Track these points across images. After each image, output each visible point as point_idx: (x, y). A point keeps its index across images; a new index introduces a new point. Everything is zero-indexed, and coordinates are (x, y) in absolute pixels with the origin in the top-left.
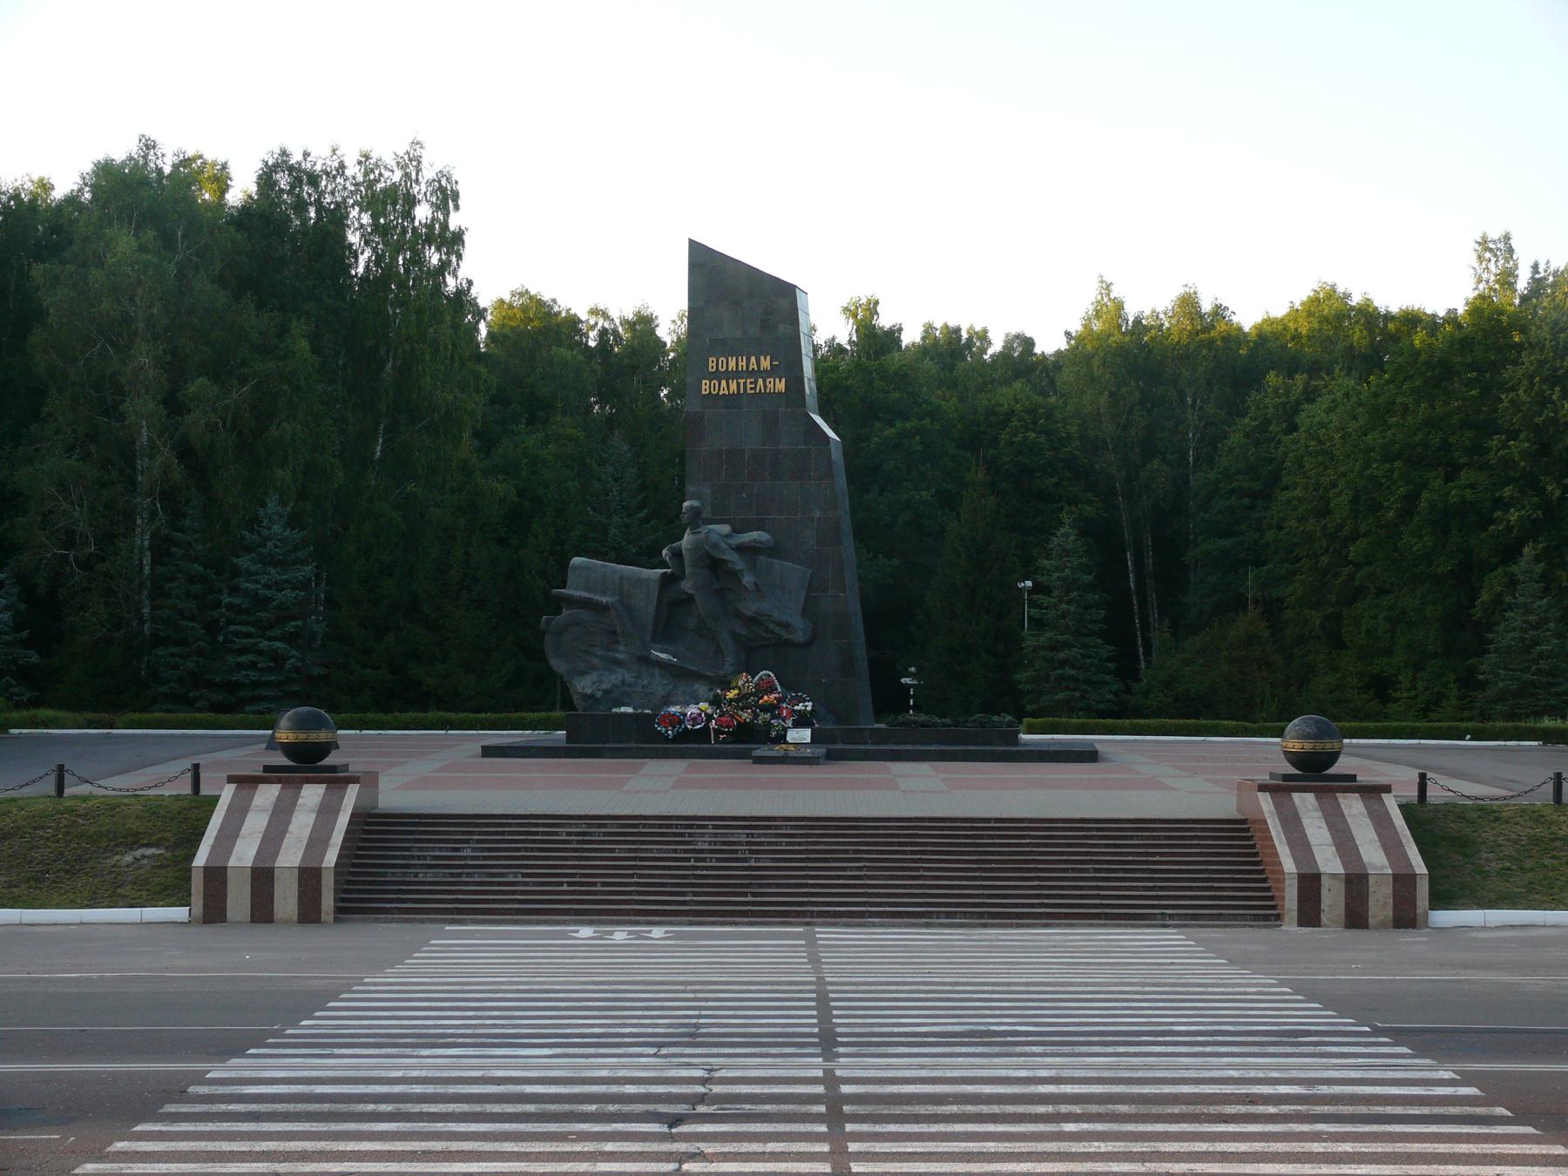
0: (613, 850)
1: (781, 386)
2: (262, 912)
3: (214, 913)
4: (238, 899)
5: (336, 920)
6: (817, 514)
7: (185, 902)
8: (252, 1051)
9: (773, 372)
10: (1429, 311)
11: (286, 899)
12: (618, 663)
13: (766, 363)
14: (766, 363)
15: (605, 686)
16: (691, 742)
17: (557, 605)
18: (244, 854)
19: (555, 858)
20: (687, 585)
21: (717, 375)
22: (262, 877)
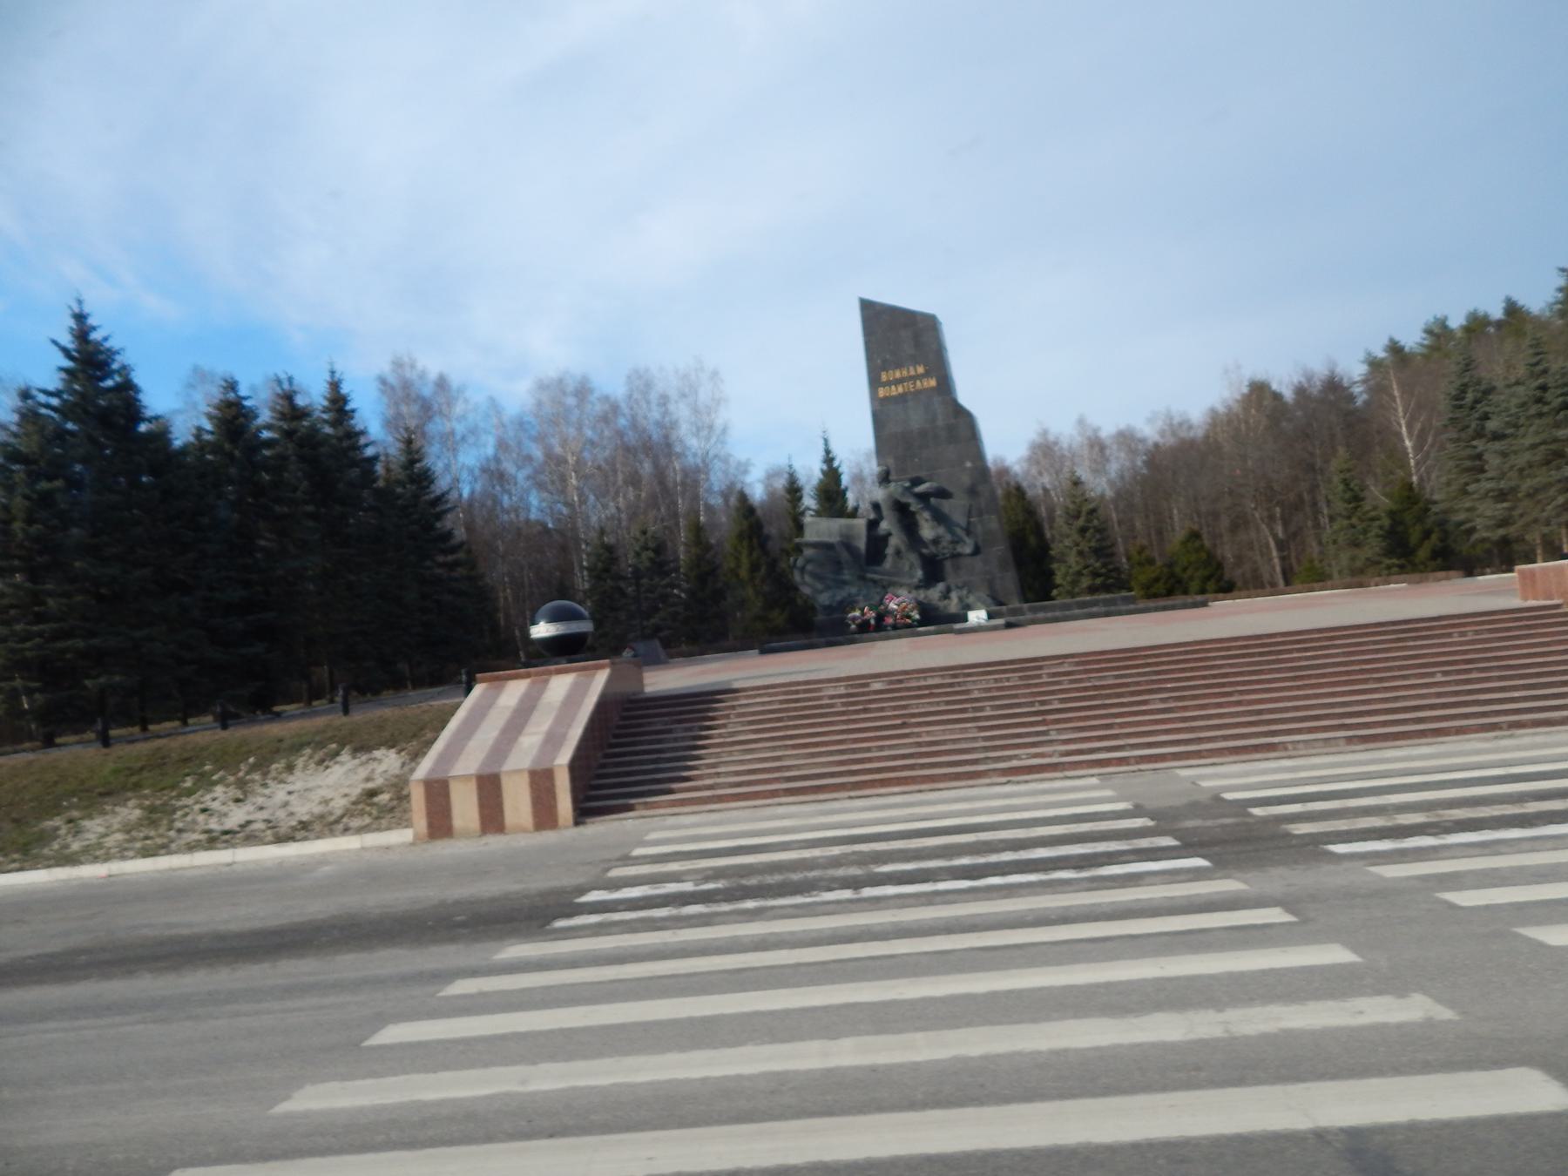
0: (869, 750)
1: (933, 383)
2: (492, 817)
3: (440, 825)
4: (465, 807)
5: (577, 823)
6: (969, 464)
7: (408, 824)
8: (560, 923)
9: (927, 374)
10: (1245, 390)
11: (517, 802)
12: (845, 583)
13: (921, 370)
14: (921, 370)
15: (839, 598)
16: (904, 627)
17: (798, 549)
18: (470, 762)
19: (821, 725)
20: (884, 526)
21: (889, 383)
22: (489, 787)
